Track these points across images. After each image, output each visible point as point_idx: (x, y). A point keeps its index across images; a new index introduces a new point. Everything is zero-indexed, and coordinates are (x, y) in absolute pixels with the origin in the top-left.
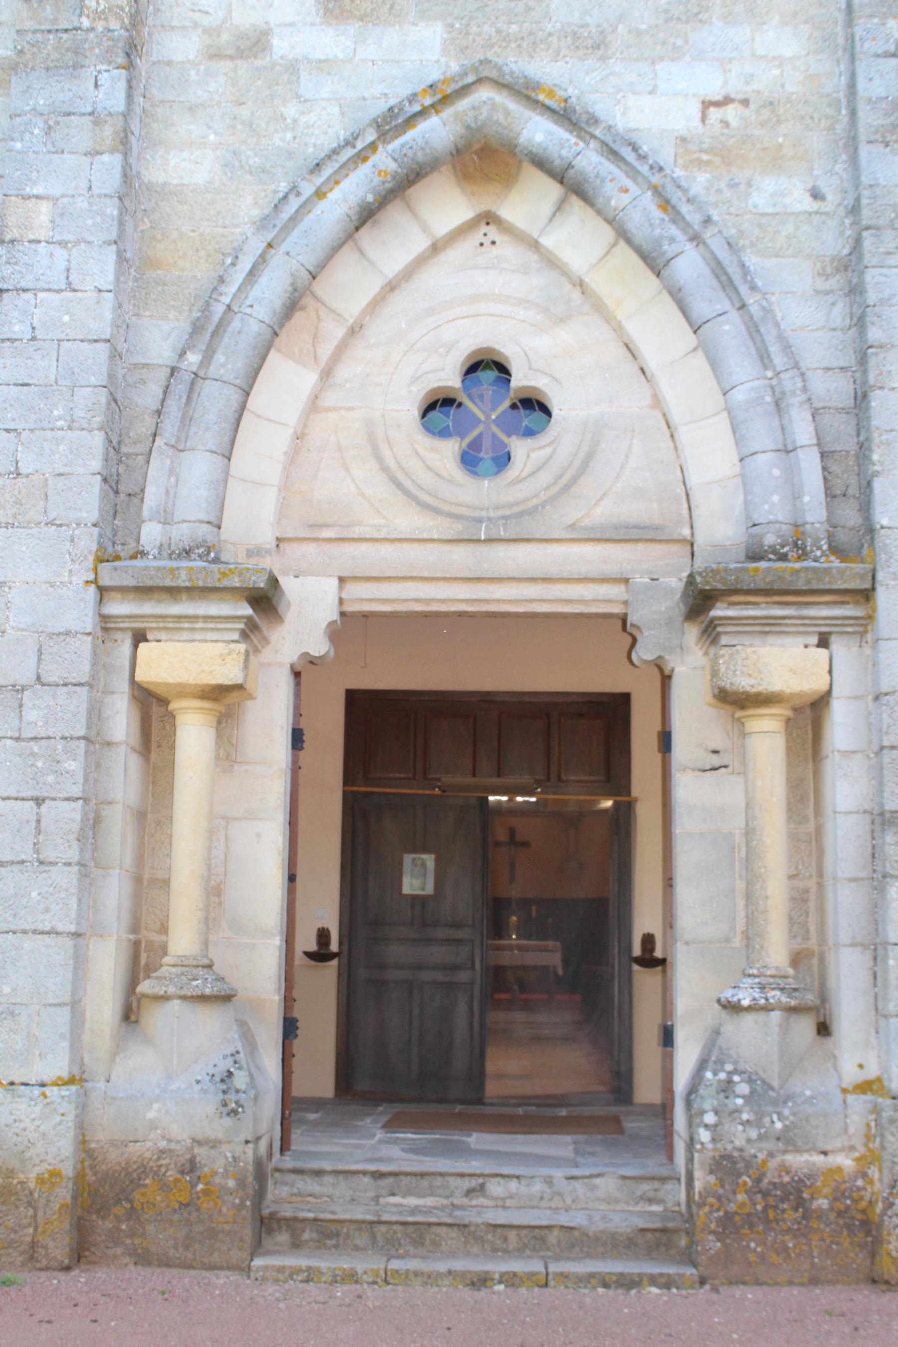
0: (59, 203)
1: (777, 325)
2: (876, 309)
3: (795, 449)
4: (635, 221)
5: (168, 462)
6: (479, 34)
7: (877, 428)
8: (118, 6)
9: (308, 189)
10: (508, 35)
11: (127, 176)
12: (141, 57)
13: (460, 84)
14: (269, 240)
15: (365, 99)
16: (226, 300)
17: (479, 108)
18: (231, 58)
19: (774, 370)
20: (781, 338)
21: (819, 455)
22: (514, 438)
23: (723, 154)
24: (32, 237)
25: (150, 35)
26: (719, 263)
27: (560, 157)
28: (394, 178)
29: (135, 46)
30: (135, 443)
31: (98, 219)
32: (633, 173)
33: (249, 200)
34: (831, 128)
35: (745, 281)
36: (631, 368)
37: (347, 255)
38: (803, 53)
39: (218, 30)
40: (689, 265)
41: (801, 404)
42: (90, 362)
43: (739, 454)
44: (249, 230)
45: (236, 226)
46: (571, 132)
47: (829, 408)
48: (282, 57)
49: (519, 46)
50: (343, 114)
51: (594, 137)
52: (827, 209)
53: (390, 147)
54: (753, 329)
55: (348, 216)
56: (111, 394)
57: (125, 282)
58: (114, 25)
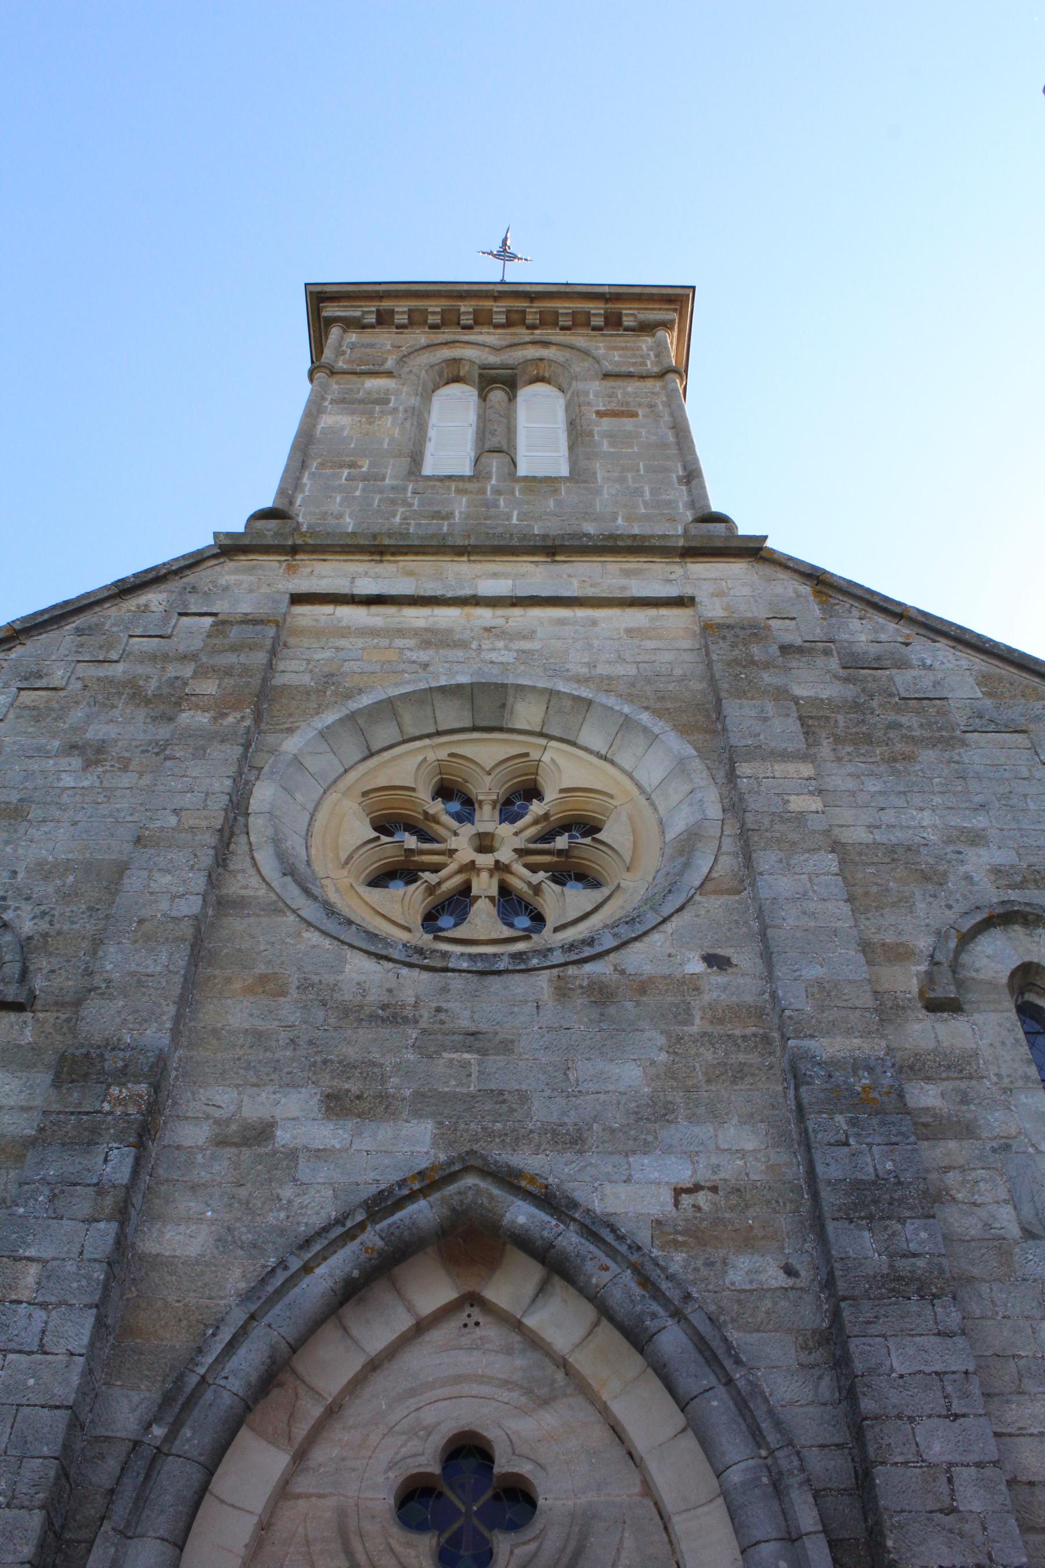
0: (49, 1266)
1: (766, 1400)
2: (865, 1379)
3: (800, 1537)
4: (616, 1297)
5: (113, 1550)
6: (467, 1131)
7: (886, 1509)
8: (138, 1095)
9: (295, 1264)
10: (493, 1132)
11: (121, 1243)
12: (153, 1141)
13: (447, 1172)
14: (252, 1311)
15: (358, 1184)
16: (202, 1371)
17: (465, 1193)
18: (236, 1145)
19: (768, 1448)
20: (771, 1412)
21: (827, 1545)
22: (496, 1531)
23: (697, 1235)
24: (14, 1297)
25: (165, 1123)
26: (702, 1338)
27: (542, 1237)
28: (380, 1255)
29: (149, 1130)
30: (80, 1528)
31: (84, 1283)
32: (612, 1253)
33: (238, 1272)
34: (796, 1210)
35: (730, 1355)
36: (618, 1452)
37: (330, 1332)
38: (763, 1147)
39: (228, 1121)
40: (671, 1340)
41: (801, 1484)
42: (46, 1430)
43: (739, 1543)
44: (233, 1301)
45: (222, 1298)
46: (552, 1216)
47: (831, 1490)
48: (283, 1146)
49: (503, 1140)
50: (336, 1197)
51: (574, 1220)
52: (802, 1285)
53: (378, 1227)
54: (742, 1405)
55: (332, 1290)
56: (63, 1468)
57: (101, 1349)
58: (132, 1110)
